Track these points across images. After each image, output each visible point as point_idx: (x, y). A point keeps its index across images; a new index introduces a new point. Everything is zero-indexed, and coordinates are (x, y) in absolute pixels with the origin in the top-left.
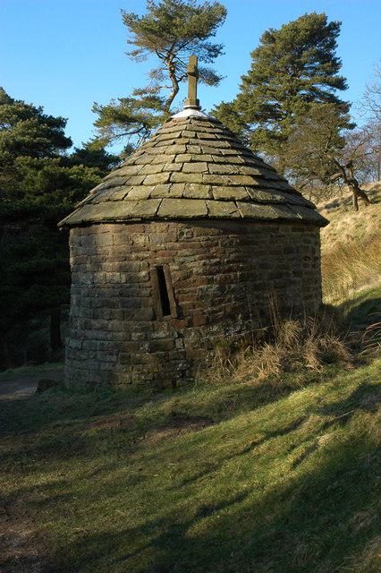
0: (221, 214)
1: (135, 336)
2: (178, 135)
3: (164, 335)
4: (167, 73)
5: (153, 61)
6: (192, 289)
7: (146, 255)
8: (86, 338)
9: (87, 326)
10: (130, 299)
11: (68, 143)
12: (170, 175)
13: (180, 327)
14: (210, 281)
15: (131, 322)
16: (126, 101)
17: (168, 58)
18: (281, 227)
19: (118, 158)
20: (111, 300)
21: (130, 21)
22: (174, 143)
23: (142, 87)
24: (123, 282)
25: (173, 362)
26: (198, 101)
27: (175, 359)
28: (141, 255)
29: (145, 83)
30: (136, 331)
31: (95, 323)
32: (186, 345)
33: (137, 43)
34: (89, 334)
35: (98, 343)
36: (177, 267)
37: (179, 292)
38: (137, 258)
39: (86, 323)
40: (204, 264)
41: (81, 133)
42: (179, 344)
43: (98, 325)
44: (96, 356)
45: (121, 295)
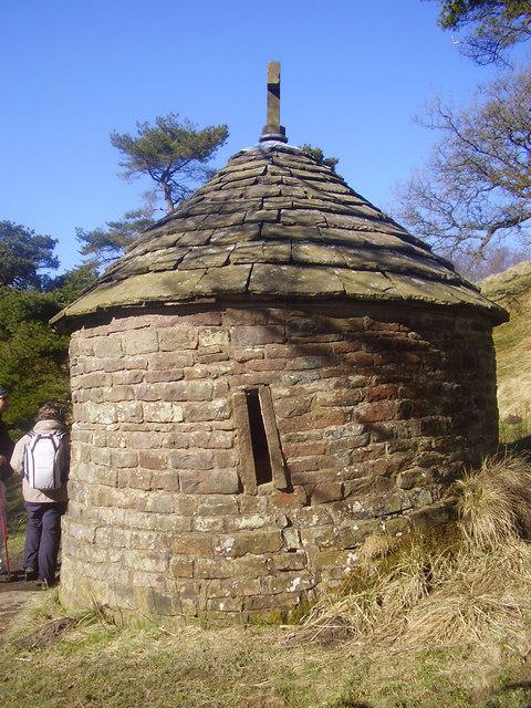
0: (369, 292)
1: (202, 523)
2: (261, 170)
3: (261, 522)
4: (162, 194)
5: (146, 182)
6: (315, 432)
7: (224, 369)
8: (101, 524)
9: (102, 500)
10: (191, 452)
11: (55, 264)
12: (261, 226)
13: (291, 505)
14: (347, 417)
15: (193, 497)
16: (118, 226)
17: (162, 180)
18: (459, 320)
19: (68, 334)
20: (153, 453)
21: (123, 143)
22: (256, 182)
23: (136, 209)
24: (176, 419)
25: (282, 575)
26: (282, 130)
27: (285, 570)
28: (213, 368)
29: (137, 204)
30: (204, 513)
31: (119, 496)
32: (305, 542)
33: (128, 166)
34: (108, 515)
35: (128, 534)
36: (285, 392)
37: (289, 440)
38: (206, 375)
39: (102, 496)
40: (139, 421)
41: (69, 258)
42: (291, 539)
43: (126, 501)
44: (122, 559)
45: (173, 444)
